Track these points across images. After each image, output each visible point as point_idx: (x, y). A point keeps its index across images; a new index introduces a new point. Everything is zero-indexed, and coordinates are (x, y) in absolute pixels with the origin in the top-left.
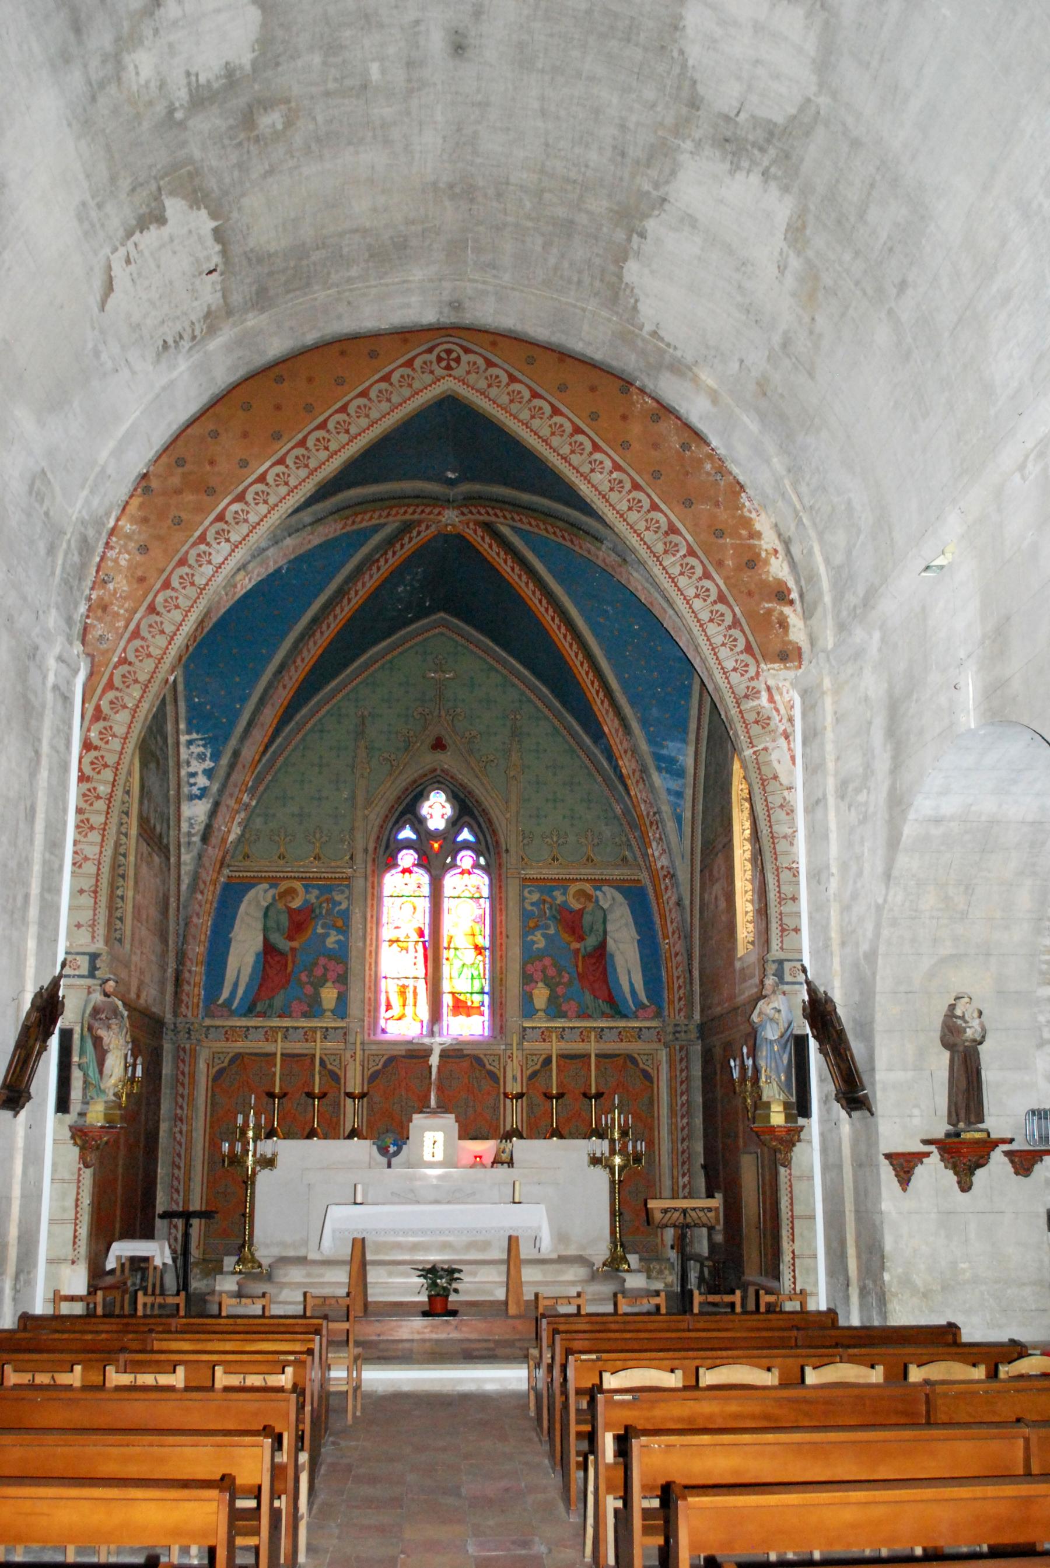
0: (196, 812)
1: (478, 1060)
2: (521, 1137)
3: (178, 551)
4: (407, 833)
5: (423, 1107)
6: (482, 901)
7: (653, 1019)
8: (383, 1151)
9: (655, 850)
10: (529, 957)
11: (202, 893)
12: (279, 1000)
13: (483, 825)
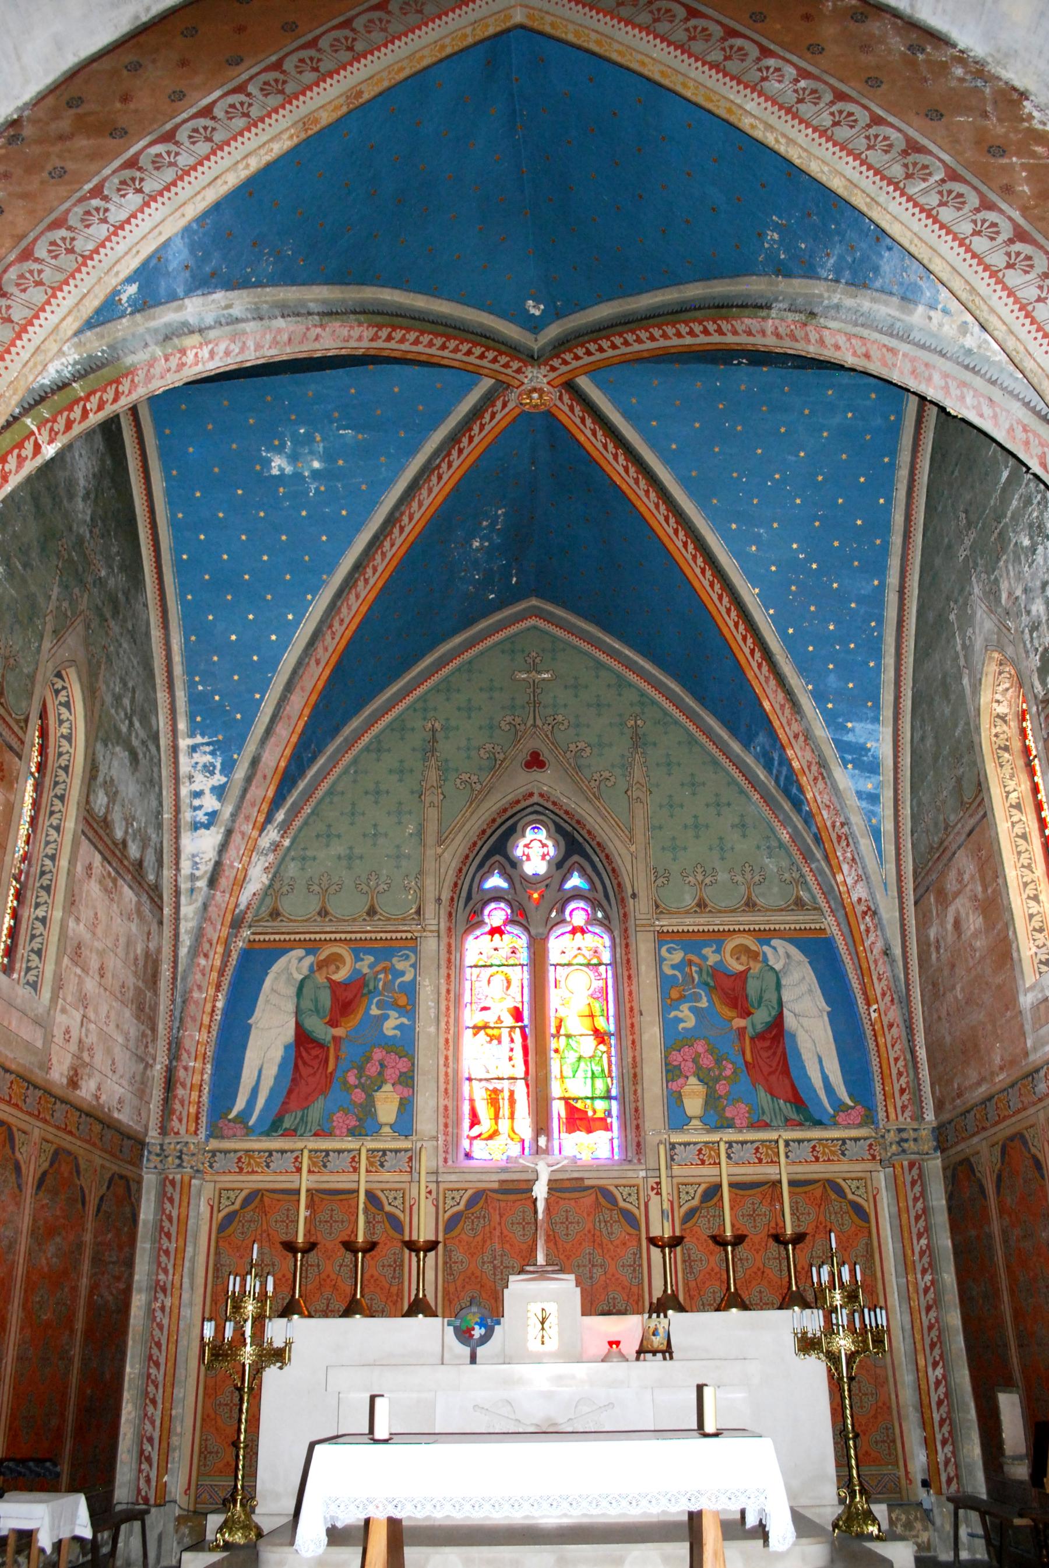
0: (200, 846)
1: (604, 1192)
2: (681, 1309)
3: (52, 210)
4: (495, 881)
5: (524, 1264)
6: (602, 969)
7: (860, 1126)
8: (464, 1335)
9: (847, 875)
10: (674, 1041)
11: (206, 956)
12: (317, 1109)
13: (599, 866)
